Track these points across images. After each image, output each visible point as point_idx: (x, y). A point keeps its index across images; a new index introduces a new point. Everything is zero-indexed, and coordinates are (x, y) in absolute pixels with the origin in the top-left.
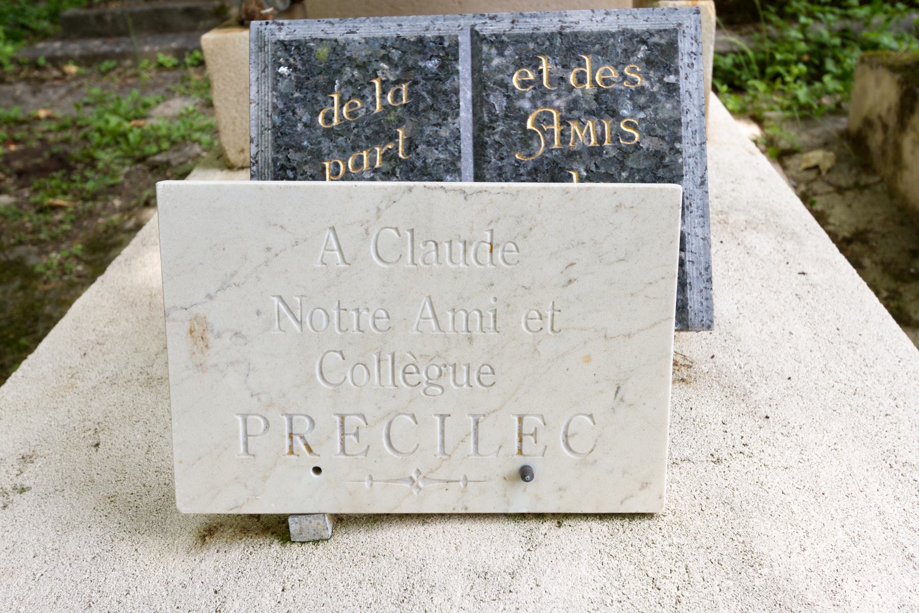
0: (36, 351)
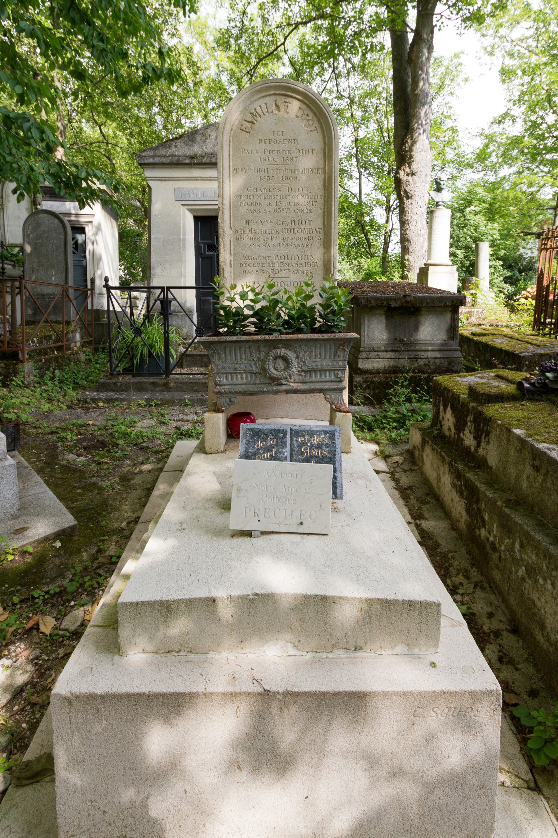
0: (60, 529)
